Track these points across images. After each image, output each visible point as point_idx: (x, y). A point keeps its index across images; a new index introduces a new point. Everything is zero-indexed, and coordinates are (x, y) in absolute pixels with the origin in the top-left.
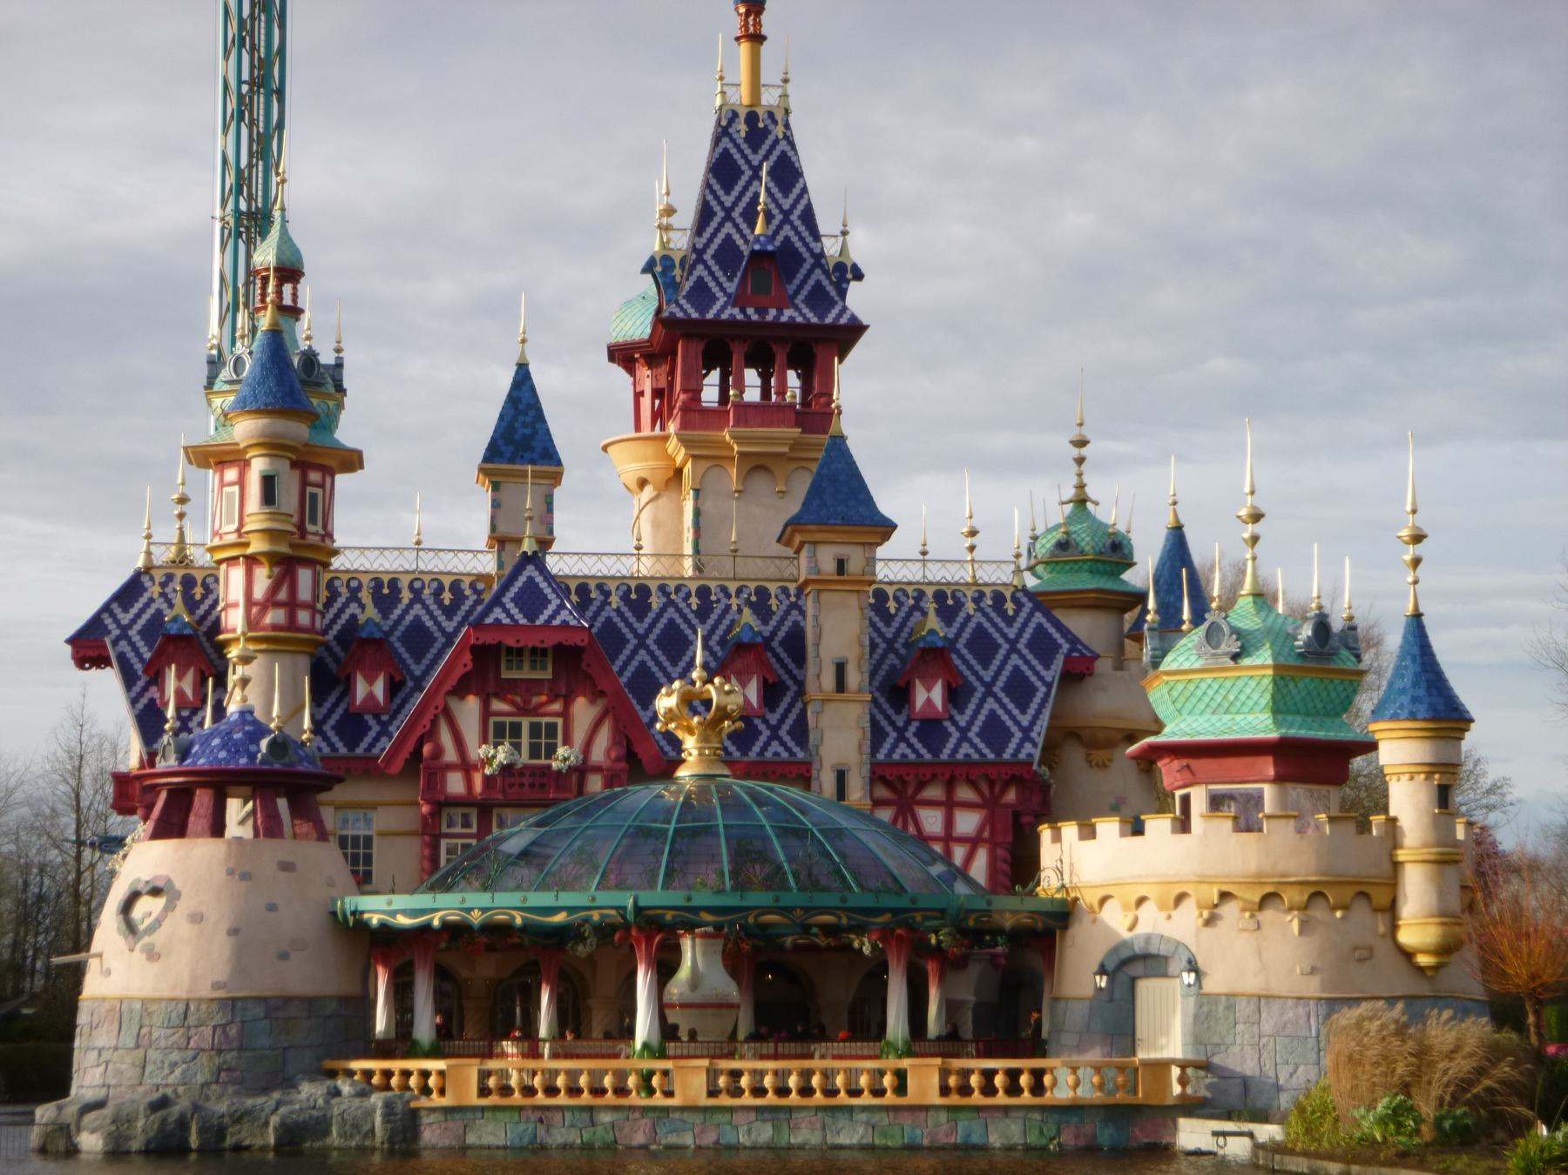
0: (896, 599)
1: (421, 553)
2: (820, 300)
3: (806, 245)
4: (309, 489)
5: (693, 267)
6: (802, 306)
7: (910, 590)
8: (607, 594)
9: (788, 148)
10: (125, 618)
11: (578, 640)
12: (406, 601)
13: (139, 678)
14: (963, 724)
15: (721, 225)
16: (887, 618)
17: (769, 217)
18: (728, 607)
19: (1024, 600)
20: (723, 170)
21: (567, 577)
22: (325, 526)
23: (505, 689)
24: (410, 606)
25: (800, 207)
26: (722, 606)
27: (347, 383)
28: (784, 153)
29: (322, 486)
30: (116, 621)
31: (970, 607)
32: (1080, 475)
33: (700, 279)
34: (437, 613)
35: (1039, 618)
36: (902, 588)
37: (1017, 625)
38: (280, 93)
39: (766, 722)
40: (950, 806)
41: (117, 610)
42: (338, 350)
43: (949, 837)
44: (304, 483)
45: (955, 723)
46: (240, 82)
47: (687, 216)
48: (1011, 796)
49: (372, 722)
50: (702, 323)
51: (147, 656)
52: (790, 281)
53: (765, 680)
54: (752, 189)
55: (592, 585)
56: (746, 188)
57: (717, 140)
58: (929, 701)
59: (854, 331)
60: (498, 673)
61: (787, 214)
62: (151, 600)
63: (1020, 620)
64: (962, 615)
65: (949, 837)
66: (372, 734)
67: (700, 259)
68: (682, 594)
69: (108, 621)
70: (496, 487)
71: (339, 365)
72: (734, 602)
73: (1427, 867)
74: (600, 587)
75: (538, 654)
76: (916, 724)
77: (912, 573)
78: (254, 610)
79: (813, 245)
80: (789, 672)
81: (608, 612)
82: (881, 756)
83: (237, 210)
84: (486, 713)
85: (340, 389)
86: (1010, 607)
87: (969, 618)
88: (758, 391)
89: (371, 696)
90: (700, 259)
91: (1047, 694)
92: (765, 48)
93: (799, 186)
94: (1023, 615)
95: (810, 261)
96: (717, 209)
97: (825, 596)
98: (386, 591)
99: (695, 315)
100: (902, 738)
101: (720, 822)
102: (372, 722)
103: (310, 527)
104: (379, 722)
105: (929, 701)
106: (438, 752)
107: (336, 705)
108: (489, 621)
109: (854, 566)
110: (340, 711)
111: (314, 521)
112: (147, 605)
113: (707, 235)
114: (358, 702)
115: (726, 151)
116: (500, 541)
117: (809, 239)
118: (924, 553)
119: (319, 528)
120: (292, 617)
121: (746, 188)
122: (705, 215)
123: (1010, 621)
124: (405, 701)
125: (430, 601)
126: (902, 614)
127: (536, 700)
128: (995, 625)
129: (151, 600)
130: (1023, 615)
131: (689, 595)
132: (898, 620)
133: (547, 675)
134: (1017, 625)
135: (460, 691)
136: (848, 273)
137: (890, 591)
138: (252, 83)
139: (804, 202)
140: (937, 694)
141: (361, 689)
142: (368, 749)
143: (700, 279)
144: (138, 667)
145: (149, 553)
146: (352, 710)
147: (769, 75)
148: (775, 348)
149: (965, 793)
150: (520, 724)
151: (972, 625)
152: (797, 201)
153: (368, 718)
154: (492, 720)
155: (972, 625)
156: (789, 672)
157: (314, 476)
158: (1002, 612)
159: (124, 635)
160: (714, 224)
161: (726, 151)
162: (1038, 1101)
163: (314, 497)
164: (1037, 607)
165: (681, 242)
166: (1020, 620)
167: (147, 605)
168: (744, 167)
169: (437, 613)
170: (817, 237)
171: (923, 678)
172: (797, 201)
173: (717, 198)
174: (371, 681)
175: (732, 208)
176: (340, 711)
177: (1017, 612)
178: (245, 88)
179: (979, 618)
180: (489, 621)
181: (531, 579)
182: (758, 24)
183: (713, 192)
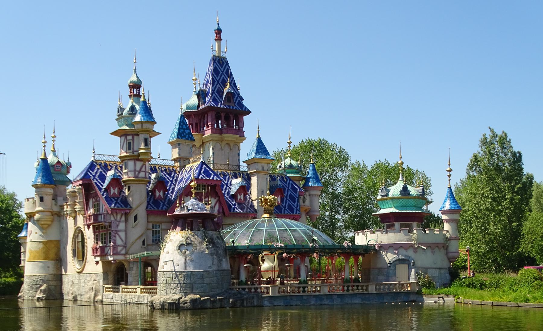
1: (160, 160)
9: (228, 68)
20: (215, 71)
25: (233, 82)
28: (228, 68)
58: (240, 199)
62: (98, 169)
73: (53, 262)
78: (137, 173)
79: (237, 91)
89: (114, 193)
92: (222, 42)
95: (237, 95)
104: (115, 200)
105: (240, 199)
113: (214, 86)
123: (286, 183)
129: (98, 169)
139: (233, 81)
146: (156, 199)
147: (223, 49)
148: (230, 115)
153: (159, 201)
158: (284, 181)
159: (94, 178)
160: (215, 84)
162: (348, 293)
173: (215, 78)
177: (287, 180)
182: (220, 36)
183: (214, 76)
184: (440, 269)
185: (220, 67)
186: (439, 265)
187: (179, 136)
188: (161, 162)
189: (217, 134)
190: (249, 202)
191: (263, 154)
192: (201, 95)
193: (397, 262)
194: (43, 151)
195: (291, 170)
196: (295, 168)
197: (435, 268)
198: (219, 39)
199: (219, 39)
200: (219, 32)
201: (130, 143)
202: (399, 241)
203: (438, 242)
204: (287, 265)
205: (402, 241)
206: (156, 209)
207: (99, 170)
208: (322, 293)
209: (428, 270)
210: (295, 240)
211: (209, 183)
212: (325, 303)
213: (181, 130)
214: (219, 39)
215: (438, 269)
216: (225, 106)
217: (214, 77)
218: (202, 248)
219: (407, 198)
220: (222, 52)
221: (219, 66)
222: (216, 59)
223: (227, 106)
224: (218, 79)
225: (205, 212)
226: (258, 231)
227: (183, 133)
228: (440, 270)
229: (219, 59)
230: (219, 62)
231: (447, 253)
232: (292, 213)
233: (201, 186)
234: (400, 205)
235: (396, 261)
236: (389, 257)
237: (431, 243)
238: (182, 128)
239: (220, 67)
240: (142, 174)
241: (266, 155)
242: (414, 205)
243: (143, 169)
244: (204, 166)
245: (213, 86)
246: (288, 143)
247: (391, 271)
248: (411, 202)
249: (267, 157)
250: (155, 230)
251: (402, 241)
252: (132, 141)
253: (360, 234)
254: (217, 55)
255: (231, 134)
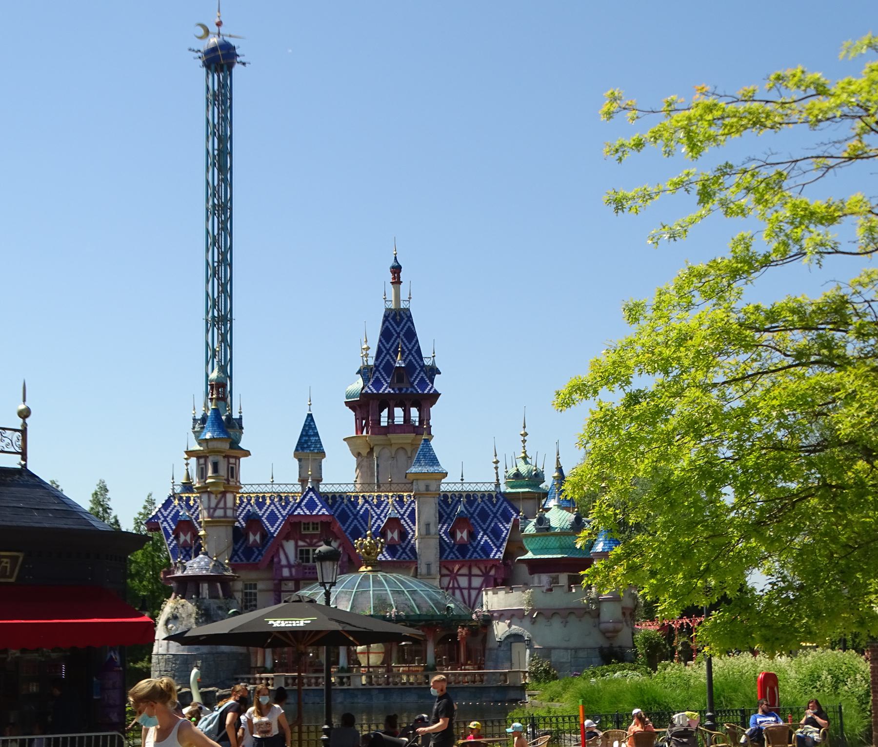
0: (451, 498)
2: (423, 384)
3: (417, 362)
4: (230, 465)
5: (374, 373)
6: (303, 508)
7: (457, 494)
8: (343, 499)
9: (411, 325)
10: (165, 514)
11: (328, 520)
12: (268, 504)
13: (171, 536)
14: (475, 545)
15: (385, 356)
16: (448, 505)
17: (403, 353)
18: (388, 502)
19: (500, 497)
20: (386, 335)
21: (328, 493)
22: (237, 479)
23: (303, 538)
24: (269, 506)
25: (416, 348)
26: (385, 502)
27: (244, 425)
28: (409, 327)
29: (235, 464)
30: (162, 515)
31: (479, 500)
32: (524, 447)
33: (377, 377)
34: (280, 508)
35: (505, 504)
36: (454, 493)
37: (497, 507)
38: (231, 265)
39: (401, 546)
40: (470, 576)
41: (162, 510)
42: (240, 413)
43: (470, 588)
44: (229, 463)
45: (472, 545)
46: (213, 262)
47: (373, 352)
48: (492, 572)
49: (255, 550)
50: (378, 394)
51: (174, 527)
52: (411, 377)
53: (400, 531)
54: (397, 341)
55: (337, 495)
56: (381, 362)
57: (384, 323)
58: (392, 538)
59: (436, 395)
60: (300, 532)
61: (410, 351)
63: (498, 505)
64: (476, 503)
65: (470, 588)
66: (256, 554)
67: (377, 370)
68: (371, 498)
69: (159, 515)
70: (300, 460)
71: (241, 418)
72: (390, 501)
74: (340, 496)
75: (315, 526)
76: (457, 546)
77: (458, 488)
78: (212, 511)
80: (410, 527)
81: (343, 506)
82: (443, 558)
83: (213, 317)
84: (297, 546)
85: (241, 428)
86: (494, 500)
87: (479, 504)
88: (402, 419)
89: (255, 541)
90: (377, 370)
91: (507, 533)
93: (415, 339)
94: (499, 503)
96: (384, 350)
97: (421, 499)
98: (261, 500)
99: (375, 392)
100: (451, 552)
101: (371, 589)
102: (255, 550)
103: (231, 480)
104: (258, 550)
105: (392, 538)
106: (280, 561)
107: (242, 544)
108: (296, 513)
109: (433, 488)
110: (244, 546)
111: (232, 477)
112: (173, 509)
113: (380, 360)
114: (251, 542)
115: (387, 327)
116: (303, 481)
117: (419, 360)
118: (462, 480)
119: (234, 480)
120: (225, 512)
121: (381, 362)
122: (379, 352)
123: (494, 505)
124: (268, 542)
125: (277, 504)
126: (453, 504)
127: (315, 541)
128: (488, 507)
130: (499, 503)
131: (373, 498)
132: (452, 506)
133: (318, 532)
134: (497, 507)
135: (287, 538)
136: (433, 371)
137: (449, 495)
138: (218, 262)
139: (417, 346)
140: (465, 535)
141: (251, 538)
142: (254, 561)
143: (377, 377)
144: (171, 532)
145: (173, 489)
147: (404, 296)
149: (475, 571)
150: (309, 550)
151: (480, 507)
152: (414, 346)
154: (299, 549)
155: (480, 507)
156: (410, 527)
157: (232, 461)
158: (492, 502)
160: (382, 356)
161: (387, 327)
163: (232, 468)
164: (505, 500)
165: (371, 362)
166: (498, 505)
167: (173, 509)
168: (394, 333)
169: (280, 508)
170: (421, 358)
171: (459, 529)
172: (414, 346)
174: (255, 535)
175: (390, 349)
176: (244, 546)
178: (216, 264)
179: (482, 504)
180: (296, 513)
181: (311, 497)
182: (399, 277)
184: (576, 650)
185: (395, 327)
186: (575, 642)
187: (299, 449)
188: (276, 489)
189: (381, 434)
190: (410, 541)
191: (426, 464)
192: (365, 372)
193: (512, 640)
194: (186, 471)
195: (519, 482)
196: (524, 478)
197: (566, 649)
198: (397, 282)
199: (397, 282)
200: (396, 270)
201: (202, 468)
202: (509, 606)
203: (571, 606)
204: (403, 643)
205: (514, 605)
206: (245, 562)
207: (176, 509)
208: (352, 687)
209: (553, 651)
210: (418, 607)
211: (311, 520)
212: (359, 701)
213: (304, 438)
214: (397, 282)
215: (571, 649)
216: (393, 389)
217: (381, 345)
218: (190, 622)
219: (545, 535)
220: (402, 302)
221: (394, 325)
222: (389, 315)
223: (396, 389)
224: (388, 346)
225: (204, 572)
226: (361, 594)
227: (306, 442)
228: (576, 652)
229: (395, 314)
230: (394, 318)
231: (597, 625)
232: (485, 558)
233: (311, 524)
234: (537, 546)
235: (508, 637)
236: (500, 629)
237: (557, 607)
238: (307, 435)
239: (395, 327)
240: (219, 513)
241: (432, 466)
242: (558, 545)
243: (222, 505)
244: (311, 494)
245: (377, 359)
246: (522, 435)
247: (501, 654)
248: (553, 542)
249: (431, 469)
250: (248, 591)
251: (514, 605)
252: (204, 466)
253: (490, 593)
254: (393, 307)
255: (401, 433)
